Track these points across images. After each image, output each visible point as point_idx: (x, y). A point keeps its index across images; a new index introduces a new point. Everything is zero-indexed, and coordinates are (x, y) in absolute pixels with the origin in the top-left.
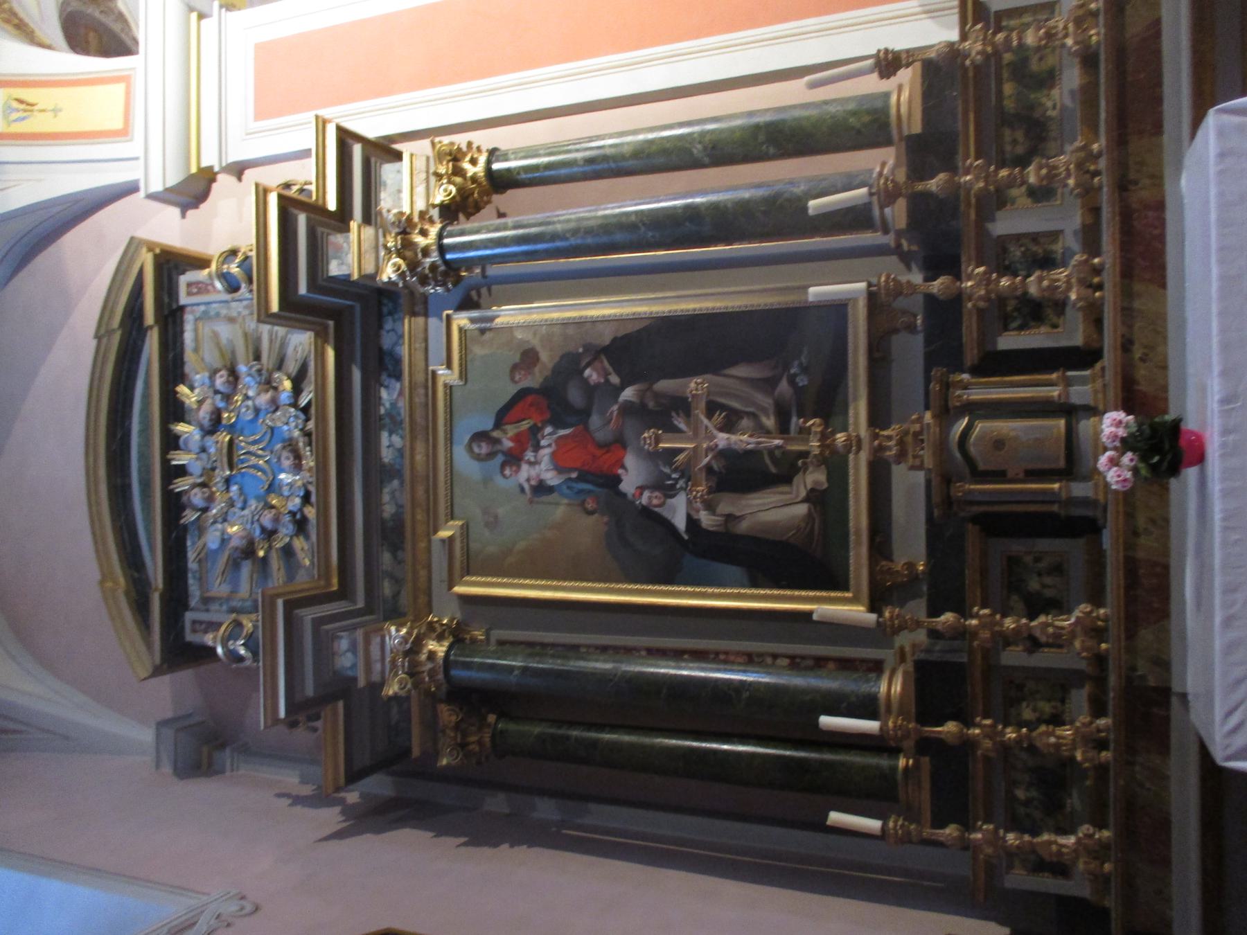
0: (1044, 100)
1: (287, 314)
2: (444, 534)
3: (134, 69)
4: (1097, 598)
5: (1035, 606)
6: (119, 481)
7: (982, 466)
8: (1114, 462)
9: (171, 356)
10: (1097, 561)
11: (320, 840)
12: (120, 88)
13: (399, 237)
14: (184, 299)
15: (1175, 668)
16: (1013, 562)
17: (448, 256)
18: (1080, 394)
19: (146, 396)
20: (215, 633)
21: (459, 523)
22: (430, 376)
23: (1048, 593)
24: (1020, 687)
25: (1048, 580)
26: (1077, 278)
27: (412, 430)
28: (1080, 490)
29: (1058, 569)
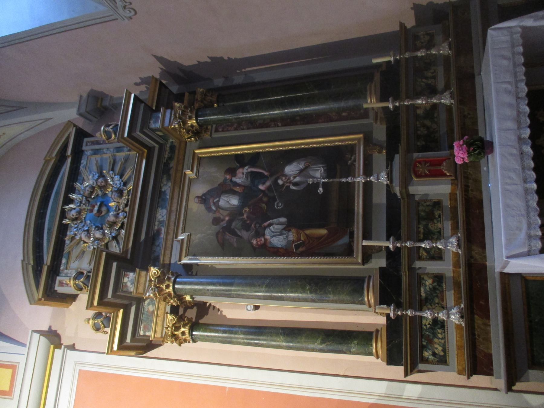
1: (129, 139)
2: (180, 238)
3: (19, 363)
6: (38, 240)
9: (56, 263)
11: (153, 55)
12: (10, 371)
13: (157, 279)
14: (84, 148)
17: (177, 286)
19: (60, 187)
20: (99, 133)
21: (187, 234)
22: (183, 174)
27: (175, 180)
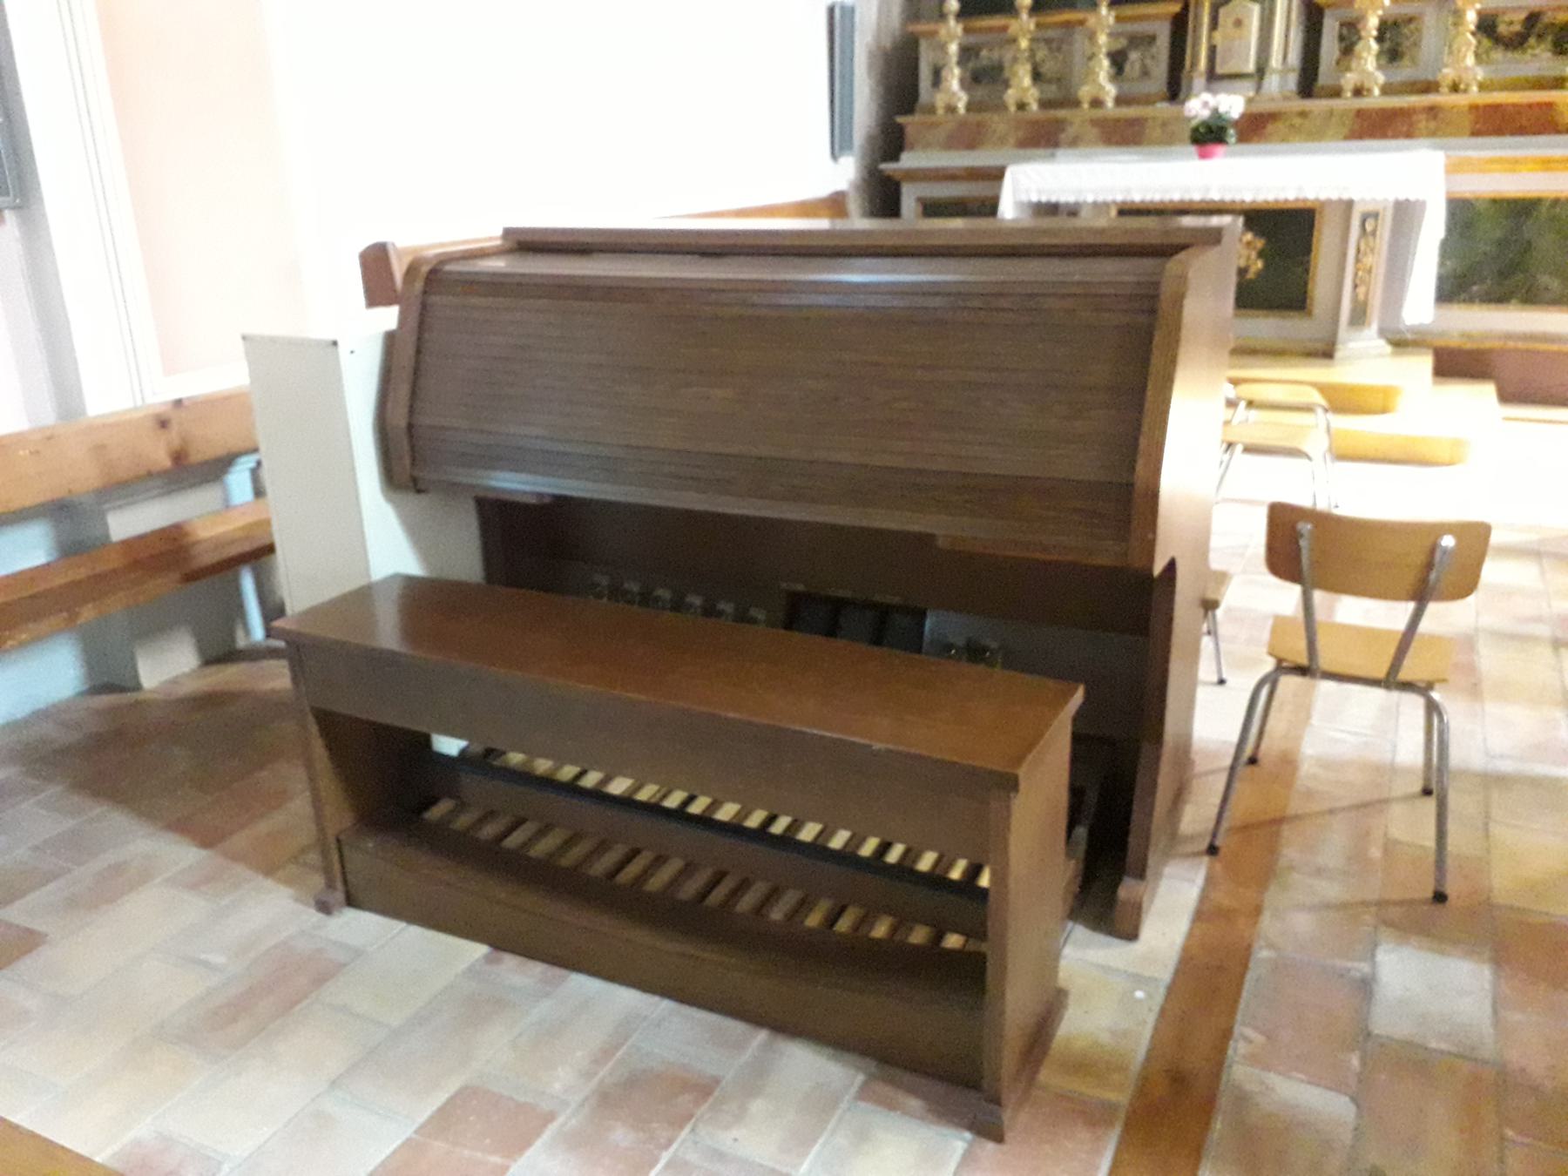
0: (1543, 46)
4: (1119, 101)
5: (1118, 60)
7: (1222, 11)
8: (1205, 104)
10: (1148, 100)
15: (1070, 151)
16: (1152, 39)
18: (1272, 83)
23: (1127, 68)
24: (1059, 49)
25: (1137, 66)
26: (960, 45)
28: (1199, 81)
29: (1145, 73)
